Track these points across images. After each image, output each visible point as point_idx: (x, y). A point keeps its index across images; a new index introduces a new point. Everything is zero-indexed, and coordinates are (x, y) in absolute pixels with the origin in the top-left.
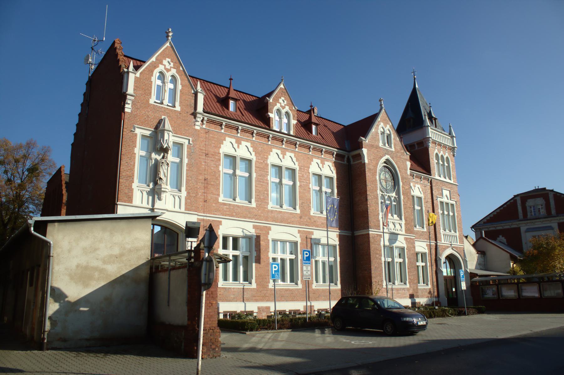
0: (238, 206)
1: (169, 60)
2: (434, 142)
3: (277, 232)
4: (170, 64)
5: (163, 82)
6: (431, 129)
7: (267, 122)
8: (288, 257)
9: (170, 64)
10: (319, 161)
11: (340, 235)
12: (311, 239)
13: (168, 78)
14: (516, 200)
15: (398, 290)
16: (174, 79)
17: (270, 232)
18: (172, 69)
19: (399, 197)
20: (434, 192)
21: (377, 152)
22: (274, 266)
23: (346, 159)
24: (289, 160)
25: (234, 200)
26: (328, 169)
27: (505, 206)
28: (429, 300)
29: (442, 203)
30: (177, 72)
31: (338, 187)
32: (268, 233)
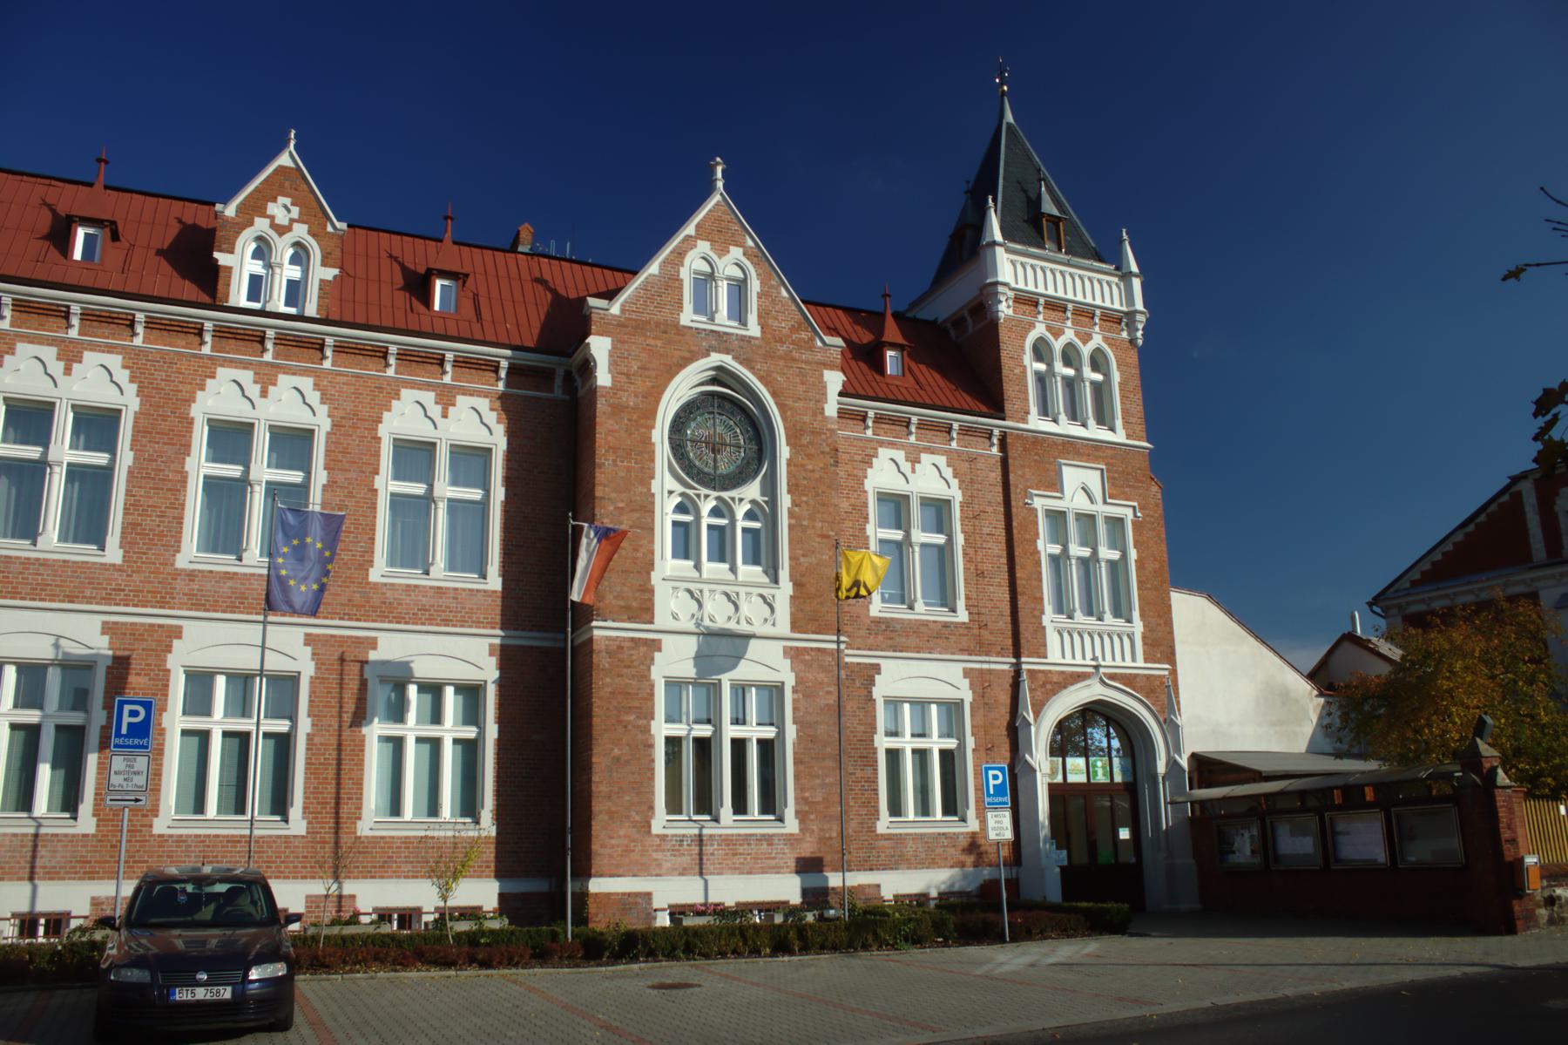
0: (45, 563)
1: (288, 201)
2: (1027, 301)
3: (210, 642)
4: (289, 211)
5: (269, 266)
6: (1008, 250)
7: (209, 280)
8: (936, 743)
9: (289, 211)
10: (900, 455)
11: (503, 648)
12: (364, 663)
13: (283, 250)
14: (1519, 495)
15: (727, 841)
16: (300, 255)
17: (176, 642)
18: (296, 225)
19: (773, 502)
20: (1012, 477)
21: (667, 345)
22: (991, 773)
23: (558, 382)
24: (293, 400)
25: (911, 608)
26: (476, 421)
27: (1482, 518)
28: (965, 876)
29: (1057, 517)
30: (309, 233)
31: (509, 481)
32: (169, 649)
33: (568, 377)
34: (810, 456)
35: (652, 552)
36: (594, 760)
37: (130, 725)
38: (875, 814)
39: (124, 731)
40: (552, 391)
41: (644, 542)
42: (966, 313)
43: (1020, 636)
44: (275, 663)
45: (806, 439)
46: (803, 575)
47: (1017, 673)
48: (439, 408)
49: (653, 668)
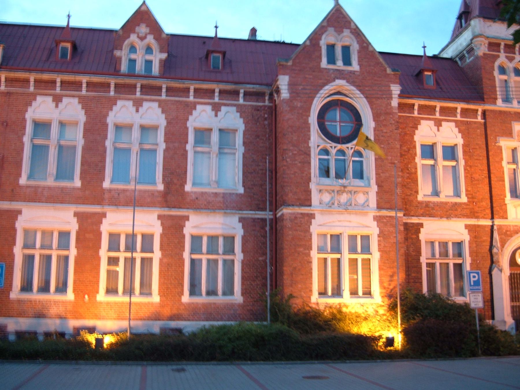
22: (472, 275)
26: (231, 118)
33: (271, 95)
34: (385, 126)
35: (310, 174)
36: (285, 268)
37: (474, 281)
38: (182, 293)
39: (472, 284)
40: (264, 102)
41: (306, 169)
42: (465, 52)
43: (495, 209)
44: (140, 229)
45: (382, 118)
46: (382, 182)
47: (492, 226)
48: (436, 128)
49: (311, 227)
